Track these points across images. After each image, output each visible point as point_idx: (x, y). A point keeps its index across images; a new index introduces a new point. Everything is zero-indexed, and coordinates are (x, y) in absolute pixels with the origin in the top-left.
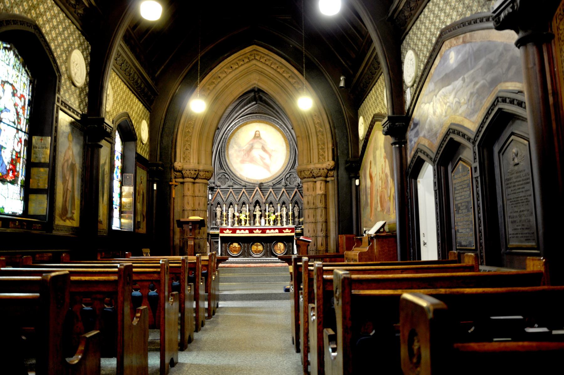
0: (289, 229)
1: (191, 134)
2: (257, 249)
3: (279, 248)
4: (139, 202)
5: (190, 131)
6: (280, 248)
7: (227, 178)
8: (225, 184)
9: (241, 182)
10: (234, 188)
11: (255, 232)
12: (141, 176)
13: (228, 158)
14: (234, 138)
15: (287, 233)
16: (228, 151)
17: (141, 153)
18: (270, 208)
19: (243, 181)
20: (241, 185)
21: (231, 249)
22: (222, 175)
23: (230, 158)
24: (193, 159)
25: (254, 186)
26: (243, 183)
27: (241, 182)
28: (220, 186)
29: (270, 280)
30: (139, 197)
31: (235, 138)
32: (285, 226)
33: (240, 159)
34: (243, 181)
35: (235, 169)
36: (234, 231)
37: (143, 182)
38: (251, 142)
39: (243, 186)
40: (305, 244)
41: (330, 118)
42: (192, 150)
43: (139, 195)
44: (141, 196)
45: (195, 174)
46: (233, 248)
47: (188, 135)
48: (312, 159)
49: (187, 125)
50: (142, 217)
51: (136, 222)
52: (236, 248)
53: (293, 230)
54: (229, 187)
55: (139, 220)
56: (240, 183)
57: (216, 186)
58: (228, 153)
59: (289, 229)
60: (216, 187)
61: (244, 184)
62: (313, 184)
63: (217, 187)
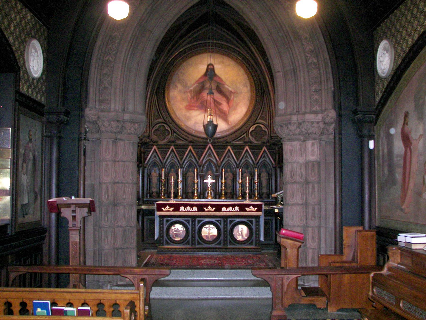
0: (254, 206)
1: (113, 63)
2: (209, 234)
3: (240, 233)
4: (26, 173)
5: (111, 59)
6: (241, 232)
7: (167, 130)
8: (165, 138)
9: (186, 136)
10: (176, 144)
11: (206, 210)
12: (30, 131)
13: (169, 101)
14: (177, 74)
15: (251, 211)
16: (169, 92)
17: (30, 93)
18: (227, 174)
19: (189, 134)
20: (186, 140)
21: (173, 232)
22: (160, 127)
23: (172, 102)
24: (115, 103)
25: (205, 142)
26: (190, 138)
27: (186, 136)
28: (156, 142)
29: (232, 294)
30: (25, 165)
31: (179, 73)
32: (247, 202)
33: (185, 104)
34: (189, 134)
35: (178, 119)
36: (177, 207)
37: (33, 140)
38: (202, 80)
39: (191, 142)
40: (295, 245)
41: (264, 67)
42: (113, 90)
43: (24, 161)
44: (30, 163)
45: (118, 126)
46: (176, 231)
47: (108, 66)
48: (149, 107)
49: (107, 50)
50: (32, 195)
51: (19, 206)
52: (179, 231)
53: (259, 208)
54: (169, 143)
55: (26, 201)
56: (186, 138)
57: (152, 140)
58: (169, 95)
59: (254, 206)
60: (152, 143)
61: (191, 140)
62: (300, 145)
63: (153, 142)
